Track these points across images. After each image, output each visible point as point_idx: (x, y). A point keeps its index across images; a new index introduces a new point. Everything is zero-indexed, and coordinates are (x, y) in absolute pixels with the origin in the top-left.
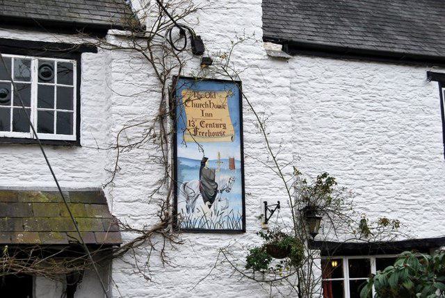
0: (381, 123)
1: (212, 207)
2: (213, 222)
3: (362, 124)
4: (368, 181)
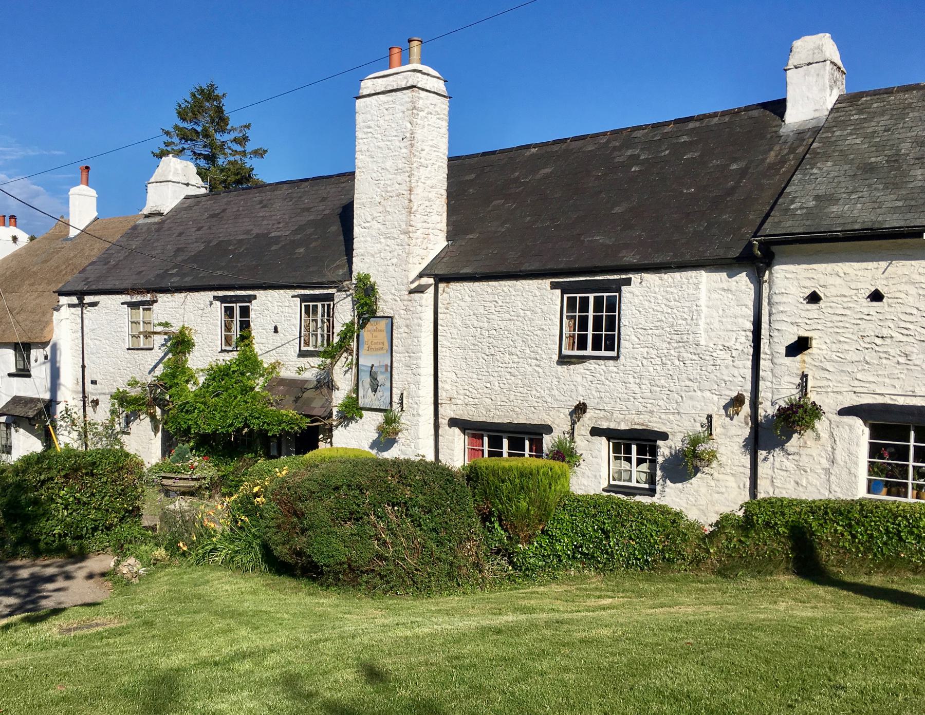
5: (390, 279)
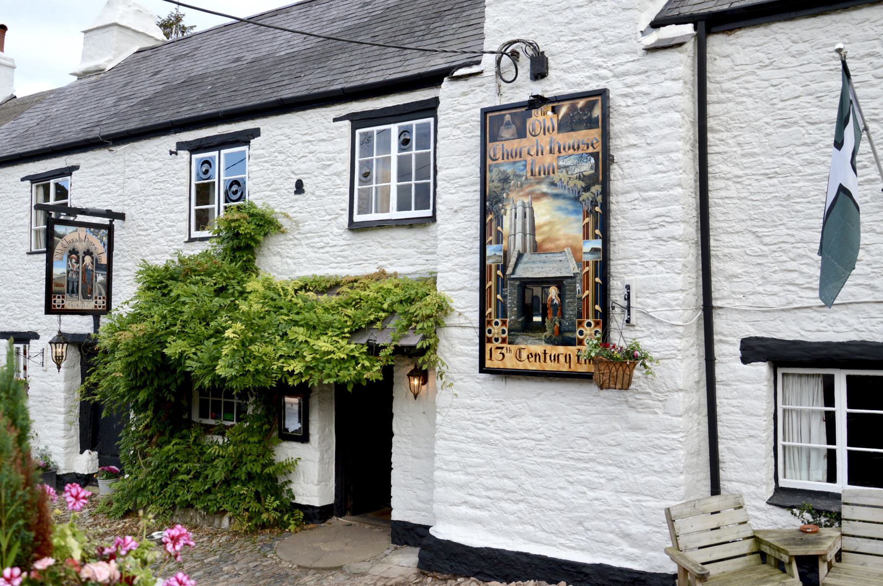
4: (878, 233)
5: (585, 35)
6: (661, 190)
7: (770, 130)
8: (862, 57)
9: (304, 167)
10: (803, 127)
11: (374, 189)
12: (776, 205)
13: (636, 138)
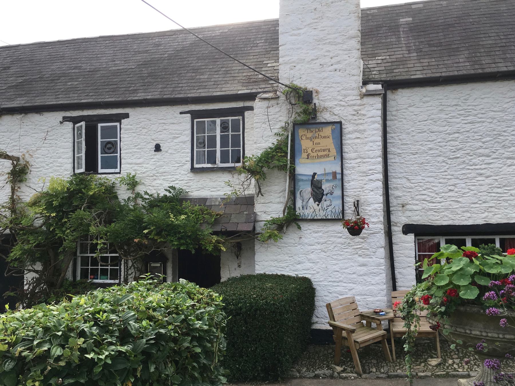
0: (476, 133)
1: (320, 205)
2: (321, 215)
3: (457, 135)
4: (460, 179)
5: (334, 85)
6: (372, 158)
7: (414, 134)
8: (453, 106)
9: (161, 137)
10: (428, 133)
11: (206, 151)
12: (417, 167)
13: (360, 135)
